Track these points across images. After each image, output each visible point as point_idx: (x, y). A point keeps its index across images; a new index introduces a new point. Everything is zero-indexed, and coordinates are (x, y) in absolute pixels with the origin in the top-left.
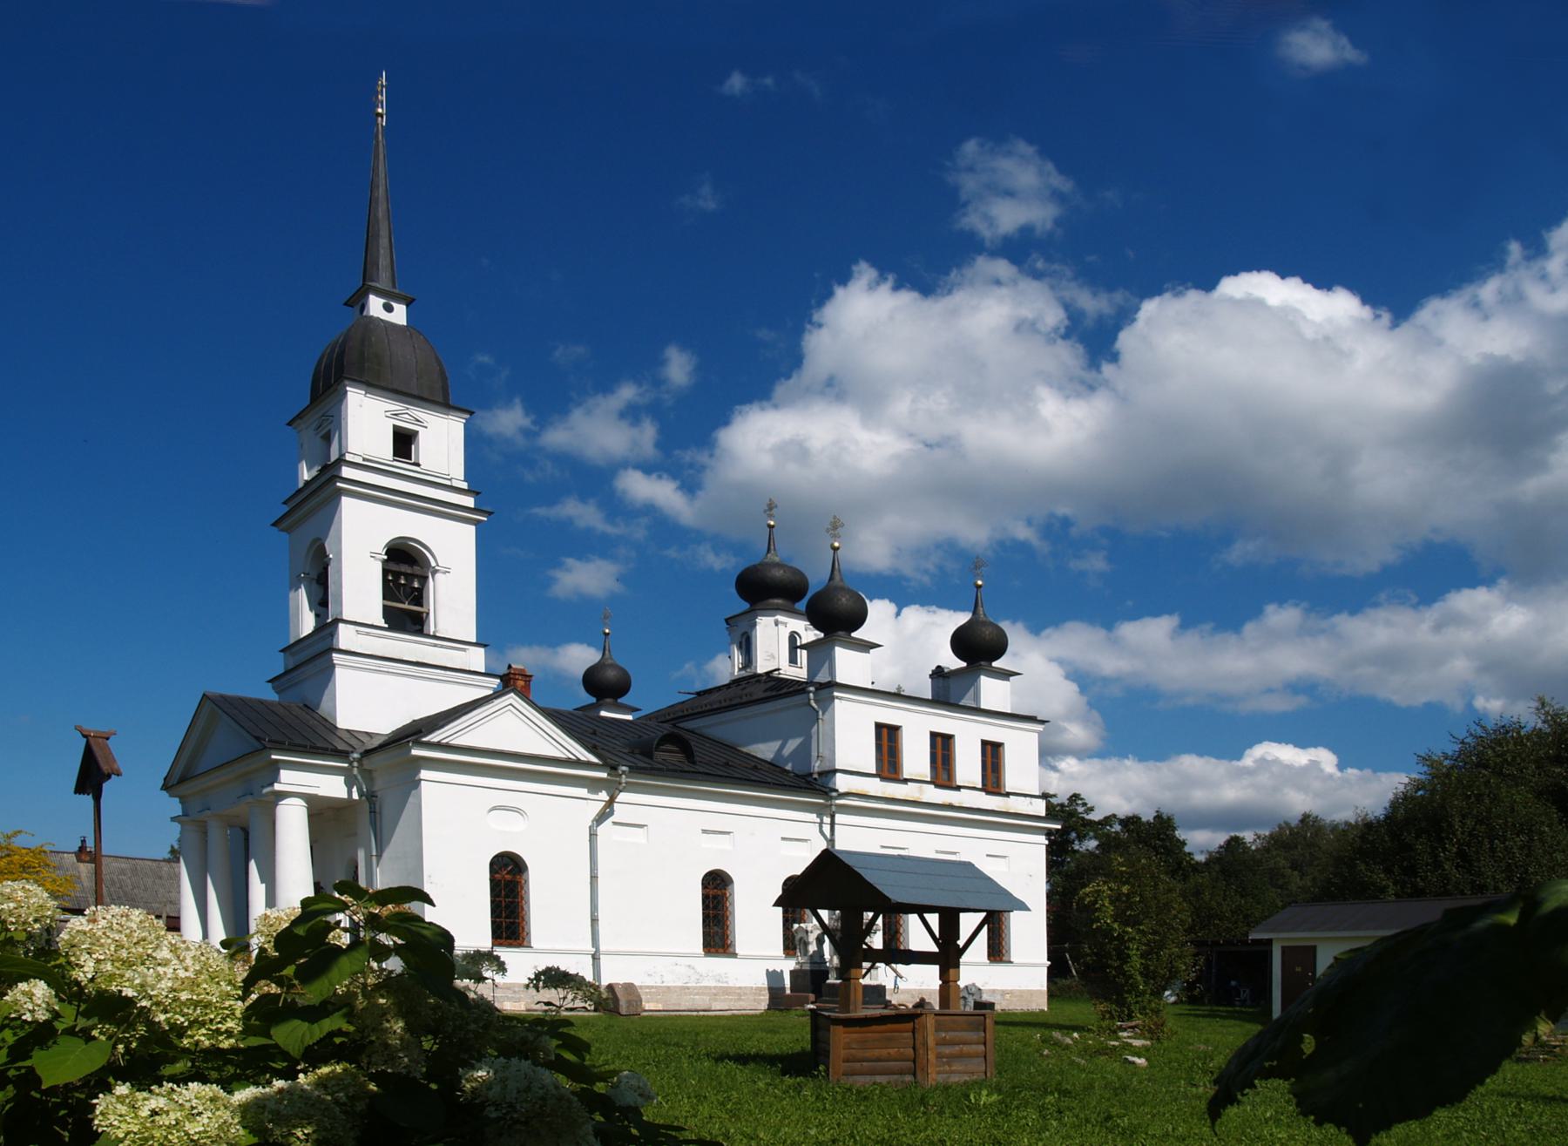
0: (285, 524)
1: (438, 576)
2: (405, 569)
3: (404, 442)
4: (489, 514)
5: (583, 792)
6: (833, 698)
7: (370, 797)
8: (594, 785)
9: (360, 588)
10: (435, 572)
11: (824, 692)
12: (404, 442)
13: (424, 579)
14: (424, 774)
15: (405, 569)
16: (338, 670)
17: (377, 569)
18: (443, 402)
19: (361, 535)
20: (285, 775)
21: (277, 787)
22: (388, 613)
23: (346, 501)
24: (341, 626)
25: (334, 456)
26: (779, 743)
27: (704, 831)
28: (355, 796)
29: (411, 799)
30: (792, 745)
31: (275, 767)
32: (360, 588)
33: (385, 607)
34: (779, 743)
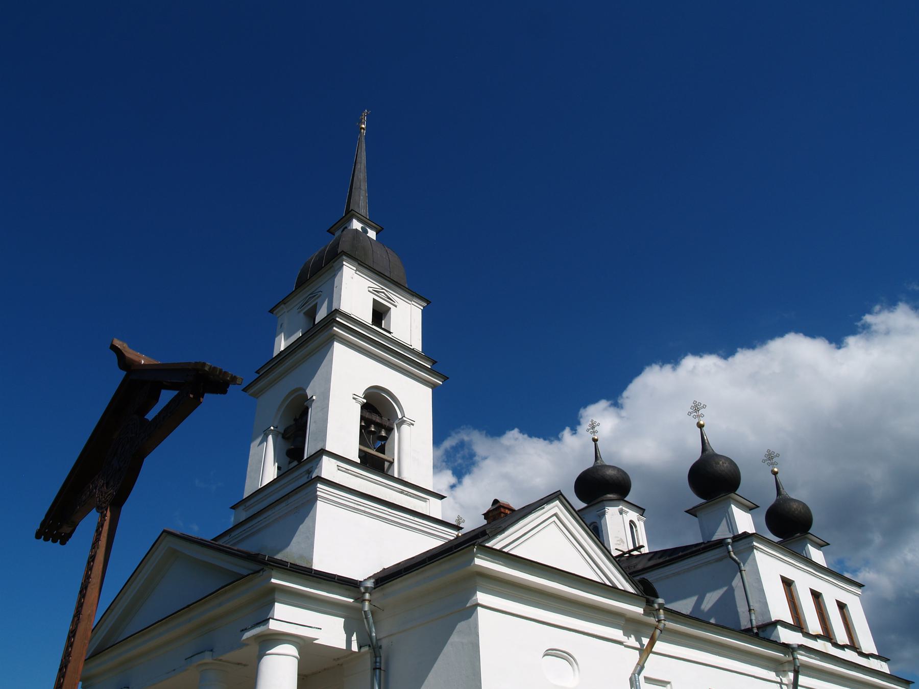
0: (252, 391)
1: (405, 427)
2: (378, 416)
3: (380, 314)
4: (445, 378)
5: (617, 634)
6: (753, 547)
7: (371, 645)
8: (630, 625)
9: (341, 430)
10: (402, 422)
11: (741, 544)
12: (380, 314)
13: (390, 430)
14: (482, 597)
15: (378, 416)
16: (320, 505)
17: (355, 412)
18: (412, 292)
19: (348, 376)
20: (281, 610)
21: (273, 625)
22: (363, 455)
23: (337, 347)
24: (325, 459)
25: (321, 314)
26: (695, 598)
27: (663, 683)
28: (355, 647)
29: (454, 638)
30: (711, 599)
31: (270, 597)
32: (341, 430)
33: (360, 450)
34: (695, 598)
